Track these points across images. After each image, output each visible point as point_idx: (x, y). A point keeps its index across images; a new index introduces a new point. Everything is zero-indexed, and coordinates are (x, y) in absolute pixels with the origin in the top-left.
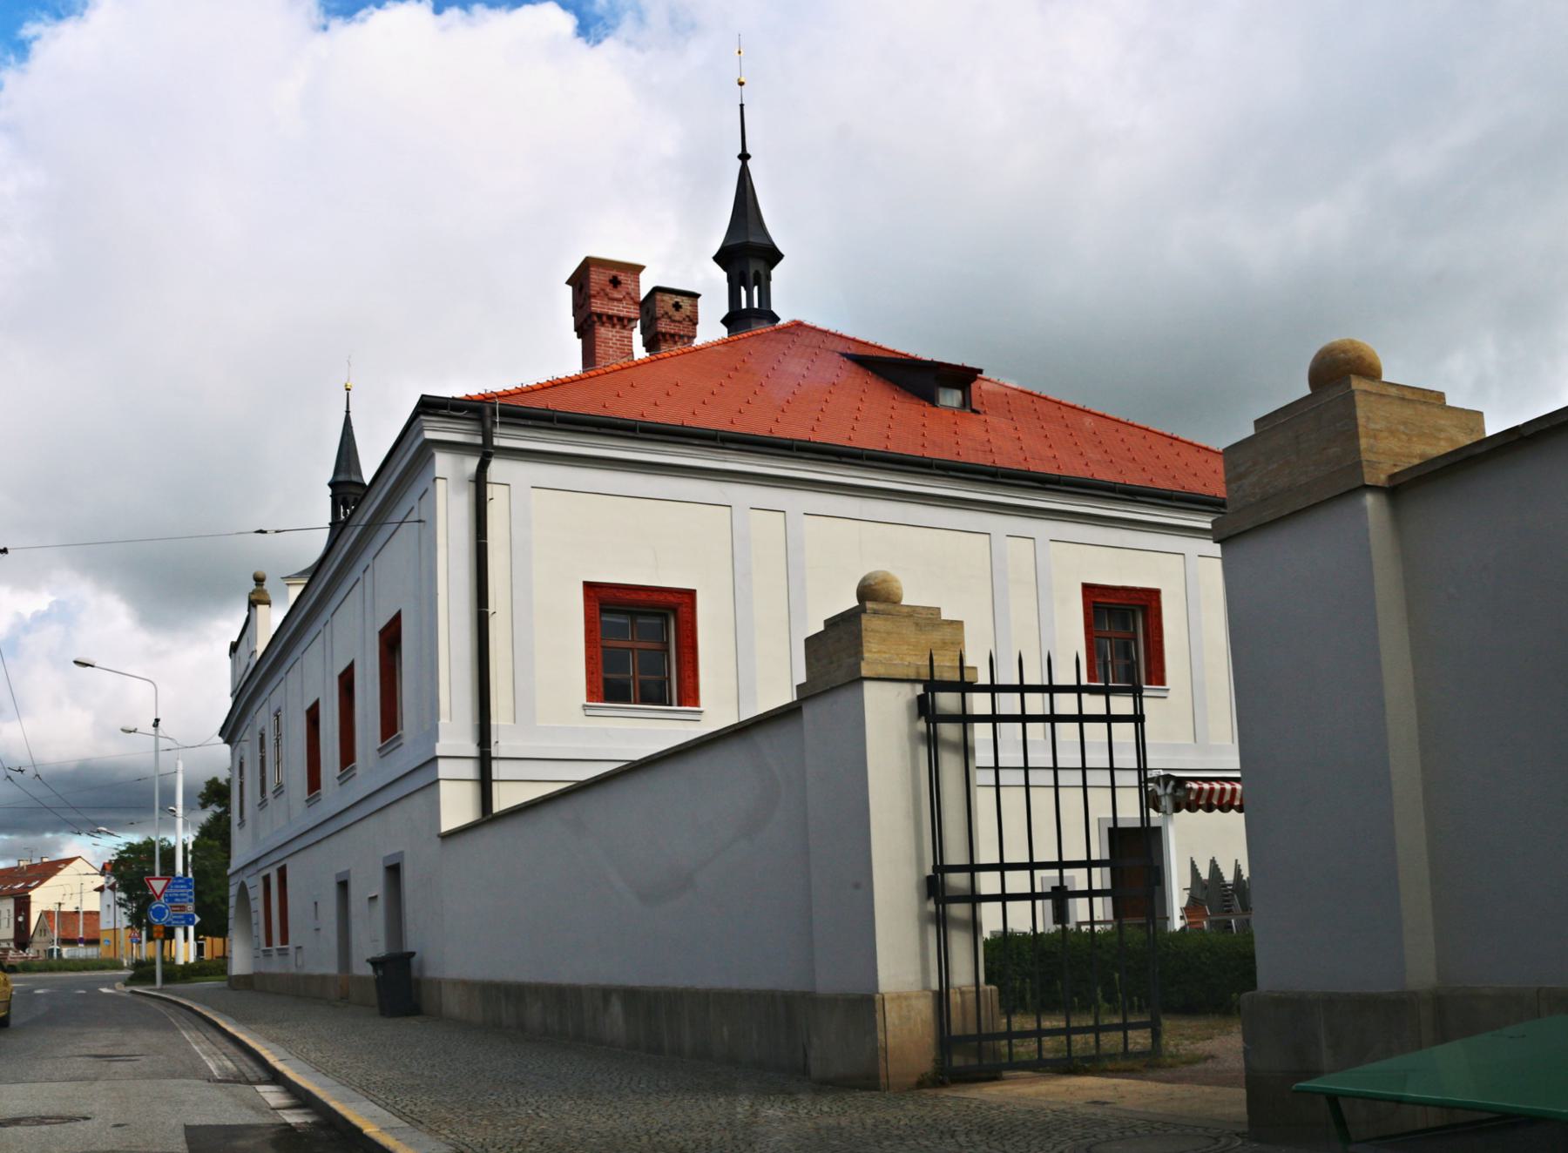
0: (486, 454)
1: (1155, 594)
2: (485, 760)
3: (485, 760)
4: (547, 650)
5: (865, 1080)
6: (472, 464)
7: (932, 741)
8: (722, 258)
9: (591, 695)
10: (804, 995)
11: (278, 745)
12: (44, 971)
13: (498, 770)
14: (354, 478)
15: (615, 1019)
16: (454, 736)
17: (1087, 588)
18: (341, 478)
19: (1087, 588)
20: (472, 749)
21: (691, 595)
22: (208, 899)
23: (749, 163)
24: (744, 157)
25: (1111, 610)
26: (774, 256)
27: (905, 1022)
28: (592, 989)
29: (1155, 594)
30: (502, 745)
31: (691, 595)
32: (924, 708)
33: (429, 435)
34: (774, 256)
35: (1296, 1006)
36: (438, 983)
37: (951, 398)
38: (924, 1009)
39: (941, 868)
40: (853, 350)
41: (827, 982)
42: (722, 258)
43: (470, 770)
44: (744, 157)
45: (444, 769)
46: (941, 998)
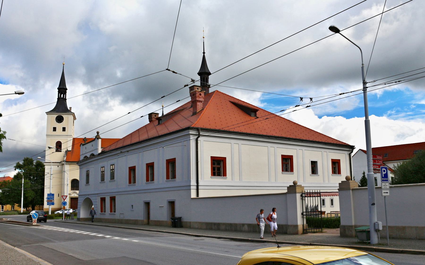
0: (199, 136)
1: (292, 156)
2: (197, 186)
3: (197, 186)
4: (206, 167)
5: (297, 233)
6: (196, 137)
7: (302, 199)
8: (199, 74)
9: (212, 175)
10: (286, 225)
11: (363, 226)
12: (3, 215)
13: (200, 187)
14: (64, 87)
15: (246, 228)
16: (193, 182)
17: (282, 155)
18: (61, 87)
19: (282, 155)
20: (196, 184)
21: (225, 158)
22: (27, 195)
23: (205, 54)
24: (204, 53)
25: (285, 159)
26: (210, 74)
27: (300, 228)
28: (240, 224)
29: (292, 156)
30: (200, 184)
31: (225, 158)
32: (301, 196)
33: (190, 133)
34: (210, 74)
35: (344, 227)
36: (186, 222)
37: (253, 114)
38: (302, 226)
39: (303, 212)
40: (232, 100)
41: (295, 224)
42: (199, 74)
43: (195, 187)
44: (204, 53)
45: (192, 187)
46: (303, 225)
